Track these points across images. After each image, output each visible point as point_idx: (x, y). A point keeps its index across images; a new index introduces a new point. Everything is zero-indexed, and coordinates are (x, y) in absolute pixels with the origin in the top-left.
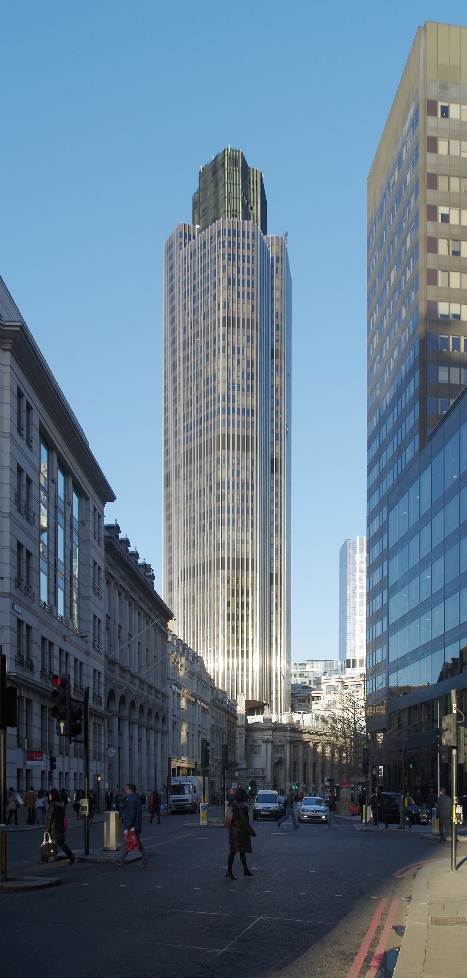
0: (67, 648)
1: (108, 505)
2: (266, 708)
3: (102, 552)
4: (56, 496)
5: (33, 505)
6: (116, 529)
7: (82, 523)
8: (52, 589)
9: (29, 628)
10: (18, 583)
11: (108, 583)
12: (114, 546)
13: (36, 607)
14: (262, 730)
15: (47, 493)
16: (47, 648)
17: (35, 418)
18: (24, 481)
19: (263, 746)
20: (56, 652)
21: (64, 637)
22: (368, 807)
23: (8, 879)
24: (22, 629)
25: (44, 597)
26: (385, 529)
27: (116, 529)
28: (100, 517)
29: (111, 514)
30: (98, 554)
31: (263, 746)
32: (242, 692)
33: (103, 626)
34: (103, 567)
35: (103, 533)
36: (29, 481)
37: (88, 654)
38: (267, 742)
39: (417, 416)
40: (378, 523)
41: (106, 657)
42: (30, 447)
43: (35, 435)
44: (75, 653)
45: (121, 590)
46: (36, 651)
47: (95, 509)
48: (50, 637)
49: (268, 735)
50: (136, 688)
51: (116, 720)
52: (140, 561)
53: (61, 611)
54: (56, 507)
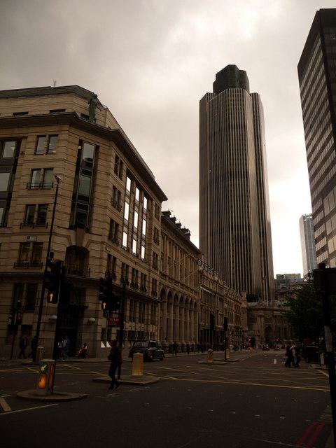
0: (137, 267)
1: (163, 202)
2: (259, 298)
3: (160, 223)
4: (143, 208)
5: (122, 203)
6: (168, 213)
7: (148, 210)
8: (130, 240)
9: (115, 258)
10: (110, 237)
11: (163, 238)
12: (168, 222)
13: (119, 248)
14: (257, 310)
15: (139, 207)
16: (125, 268)
17: (125, 167)
18: (117, 193)
19: (259, 319)
20: (130, 270)
21: (136, 263)
22: (92, 156)
23: (52, 394)
24: (111, 260)
25: (125, 244)
26: (321, 208)
27: (168, 213)
28: (158, 208)
29: (165, 207)
30: (157, 224)
31: (259, 319)
32: (245, 289)
33: (159, 258)
34: (159, 229)
35: (161, 215)
36: (119, 193)
37: (149, 271)
38: (261, 316)
39: (333, 142)
40: (317, 207)
41: (160, 272)
42: (121, 179)
43: (124, 173)
44: (141, 270)
45: (171, 242)
46: (118, 271)
47: (156, 204)
48: (127, 262)
49: (261, 313)
50: (179, 288)
51: (183, 310)
52: (182, 227)
53: (134, 250)
54: (143, 212)
